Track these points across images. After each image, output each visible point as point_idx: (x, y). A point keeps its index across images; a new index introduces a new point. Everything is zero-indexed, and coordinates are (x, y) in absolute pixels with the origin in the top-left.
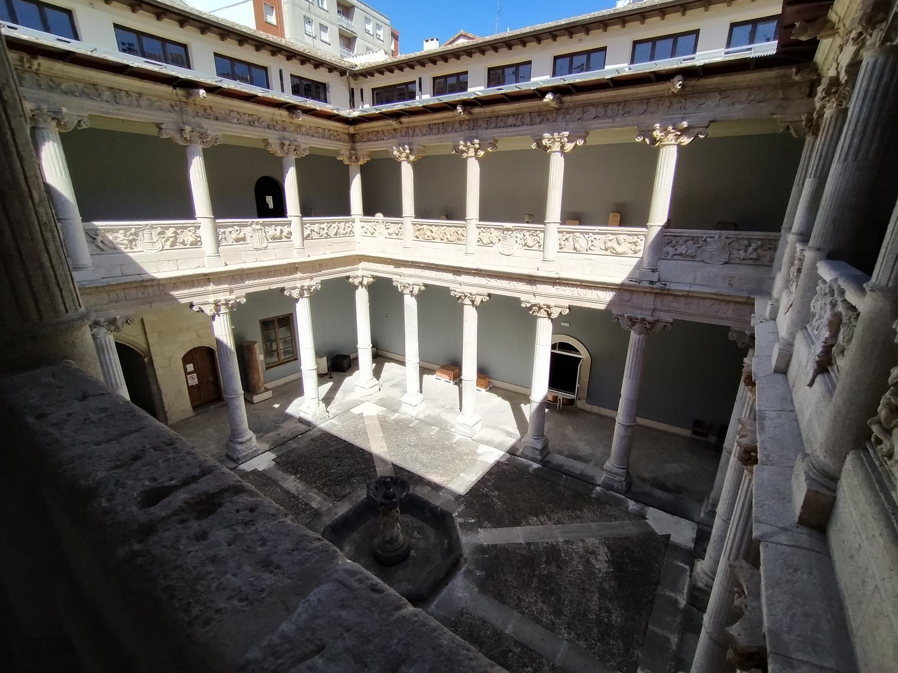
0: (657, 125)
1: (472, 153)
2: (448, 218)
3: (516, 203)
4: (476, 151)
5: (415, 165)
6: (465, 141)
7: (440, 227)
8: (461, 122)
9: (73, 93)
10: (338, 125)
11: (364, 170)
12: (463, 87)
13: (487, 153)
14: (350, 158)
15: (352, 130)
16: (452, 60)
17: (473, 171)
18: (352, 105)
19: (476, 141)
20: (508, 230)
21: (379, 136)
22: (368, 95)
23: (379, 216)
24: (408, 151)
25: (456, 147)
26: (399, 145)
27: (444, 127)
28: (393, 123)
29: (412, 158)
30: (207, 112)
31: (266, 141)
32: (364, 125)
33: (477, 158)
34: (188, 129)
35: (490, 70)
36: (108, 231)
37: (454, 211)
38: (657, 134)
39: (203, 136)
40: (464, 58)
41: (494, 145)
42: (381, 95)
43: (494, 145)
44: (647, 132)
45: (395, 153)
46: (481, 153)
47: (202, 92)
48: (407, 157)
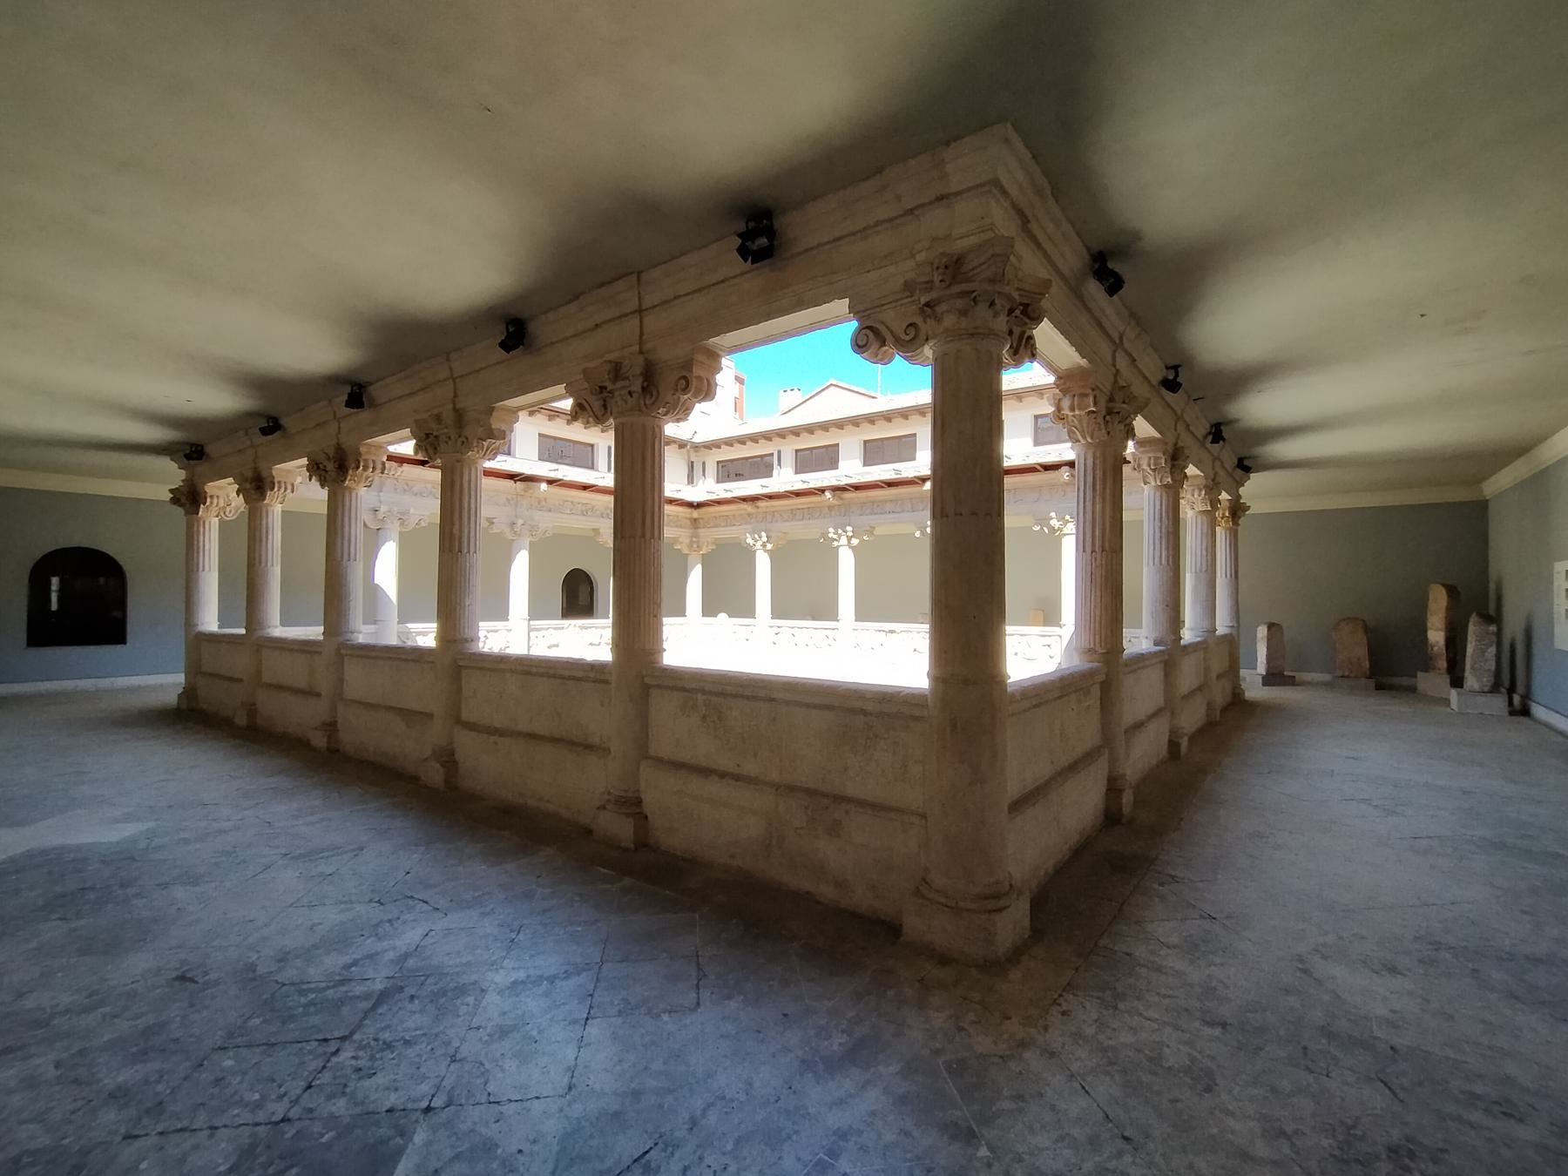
0: (1053, 514)
1: (844, 540)
2: (814, 619)
3: (805, 598)
4: (849, 539)
5: (773, 555)
6: (836, 529)
7: (805, 631)
8: (830, 508)
9: (421, 494)
10: (681, 509)
11: (707, 562)
12: (833, 463)
13: (862, 541)
14: (690, 546)
15: (695, 514)
16: (819, 432)
17: (846, 563)
18: (691, 480)
19: (849, 528)
20: (892, 632)
21: (729, 521)
22: (711, 469)
23: (723, 616)
24: (765, 539)
25: (825, 535)
26: (754, 532)
27: (810, 512)
28: (748, 507)
29: (769, 546)
30: (542, 504)
31: (596, 531)
32: (711, 509)
33: (853, 548)
34: (520, 522)
35: (865, 442)
36: (419, 634)
37: (824, 610)
38: (1055, 523)
39: (533, 529)
40: (833, 430)
41: (871, 532)
42: (729, 471)
43: (871, 532)
44: (1044, 521)
45: (750, 541)
46: (855, 542)
47: (544, 486)
48: (764, 545)
